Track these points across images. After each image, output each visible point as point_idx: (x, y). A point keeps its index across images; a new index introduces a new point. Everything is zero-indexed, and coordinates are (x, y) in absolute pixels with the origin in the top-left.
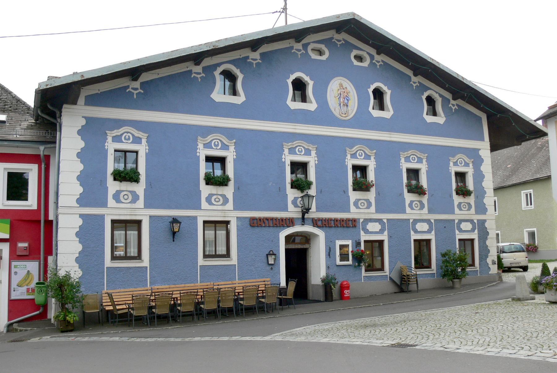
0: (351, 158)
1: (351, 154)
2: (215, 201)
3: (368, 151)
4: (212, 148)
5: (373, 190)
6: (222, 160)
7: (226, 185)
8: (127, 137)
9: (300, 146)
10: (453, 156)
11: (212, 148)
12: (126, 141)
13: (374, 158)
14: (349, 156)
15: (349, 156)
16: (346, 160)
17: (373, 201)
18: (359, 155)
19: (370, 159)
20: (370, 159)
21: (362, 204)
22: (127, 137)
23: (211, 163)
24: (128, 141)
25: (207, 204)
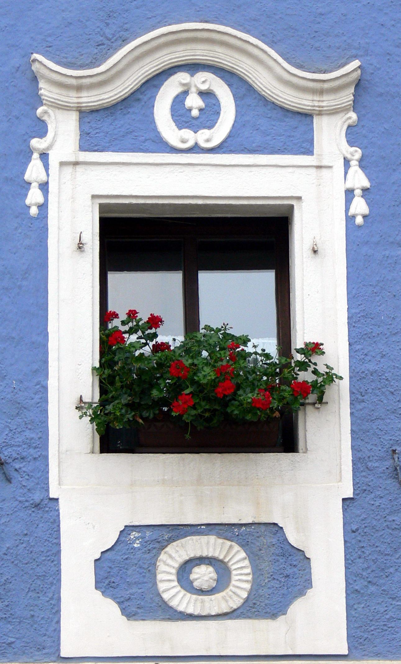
0: (89, 141)
1: (86, 115)
2: (221, 568)
3: (273, 75)
4: (161, 146)
5: (330, 436)
6: (258, 239)
7: (288, 442)
8: (194, 102)
9: (193, 67)
10: (89, 46)
11: (161, 146)
12: (190, 137)
13: (353, 135)
14: (62, 134)
15: (62, 134)
16: (34, 171)
17: (324, 544)
18: (181, 116)
19: (306, 147)
20: (306, 147)
21: (203, 575)
22: (194, 102)
23: (174, 280)
24: (203, 137)
25: (111, 608)
